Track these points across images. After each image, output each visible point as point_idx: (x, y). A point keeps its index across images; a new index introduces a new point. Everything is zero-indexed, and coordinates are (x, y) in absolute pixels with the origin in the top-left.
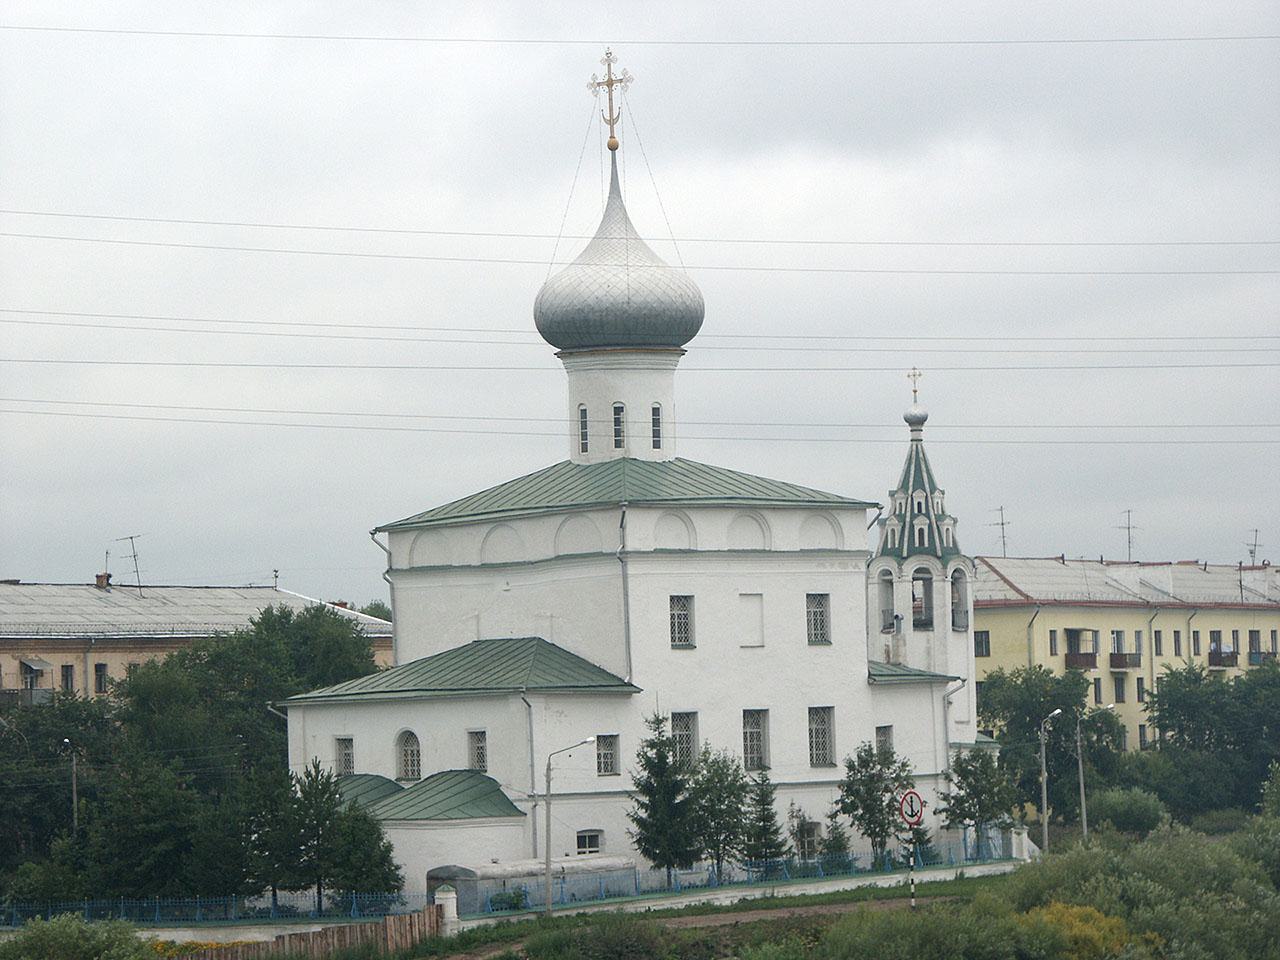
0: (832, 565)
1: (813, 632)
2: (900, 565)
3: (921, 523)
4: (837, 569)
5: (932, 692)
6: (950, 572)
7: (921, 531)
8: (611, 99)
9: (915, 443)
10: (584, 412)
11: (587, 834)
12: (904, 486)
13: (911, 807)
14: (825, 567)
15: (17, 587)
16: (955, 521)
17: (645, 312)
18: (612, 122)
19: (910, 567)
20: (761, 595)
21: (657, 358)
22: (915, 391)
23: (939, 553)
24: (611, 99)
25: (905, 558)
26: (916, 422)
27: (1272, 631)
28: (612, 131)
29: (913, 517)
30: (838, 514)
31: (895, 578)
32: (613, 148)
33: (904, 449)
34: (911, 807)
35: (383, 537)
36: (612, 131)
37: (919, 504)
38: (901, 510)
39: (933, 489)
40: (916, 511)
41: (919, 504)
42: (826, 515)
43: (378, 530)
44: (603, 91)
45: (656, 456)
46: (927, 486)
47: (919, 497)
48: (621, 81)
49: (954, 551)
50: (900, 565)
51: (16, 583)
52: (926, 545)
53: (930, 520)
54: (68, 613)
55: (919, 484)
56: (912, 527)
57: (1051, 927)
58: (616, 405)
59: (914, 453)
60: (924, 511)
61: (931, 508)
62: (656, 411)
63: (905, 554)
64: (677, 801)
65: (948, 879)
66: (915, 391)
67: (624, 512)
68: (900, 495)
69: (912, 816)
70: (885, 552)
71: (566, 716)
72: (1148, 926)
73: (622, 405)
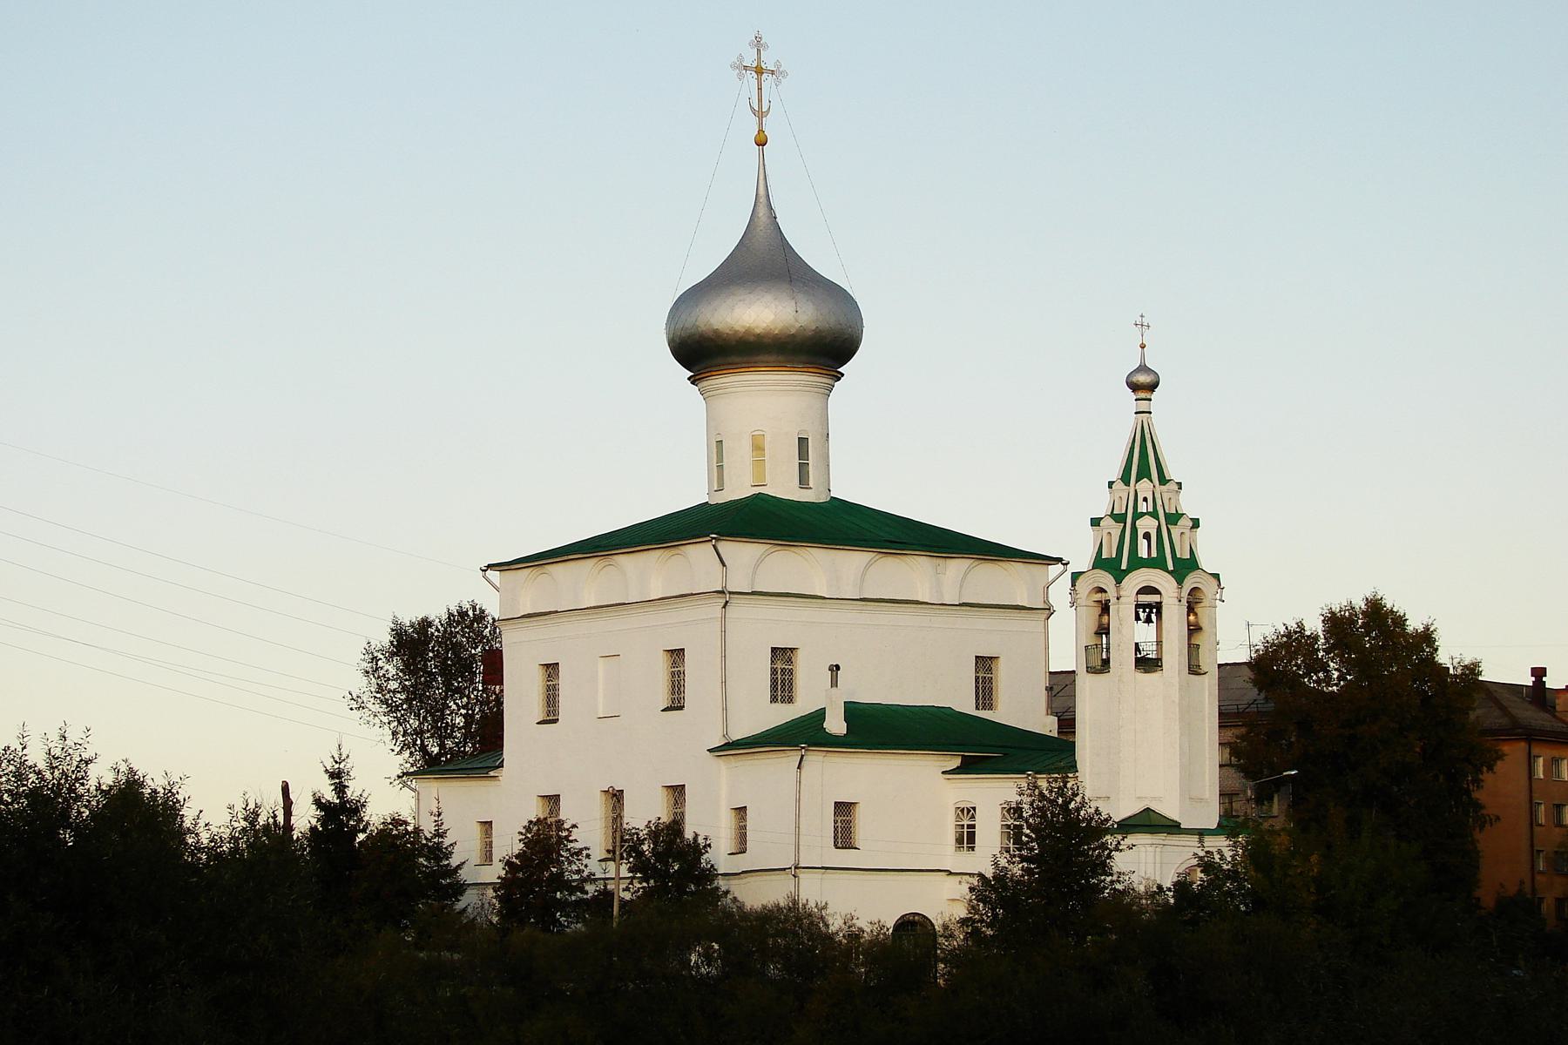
2: (1119, 582)
8: (760, 89)
10: (798, 768)
12: (1125, 478)
16: (1196, 524)
18: (760, 114)
22: (1143, 347)
23: (1171, 567)
24: (760, 89)
26: (1143, 386)
28: (761, 124)
32: (761, 143)
35: (494, 575)
36: (761, 124)
39: (1163, 480)
43: (489, 566)
44: (751, 77)
47: (1145, 488)
48: (773, 72)
50: (1119, 582)
52: (1154, 554)
53: (1158, 519)
55: (1144, 473)
56: (1134, 529)
64: (282, 823)
66: (1143, 347)
67: (802, 756)
68: (1119, 485)
70: (1100, 563)
73: (762, 433)
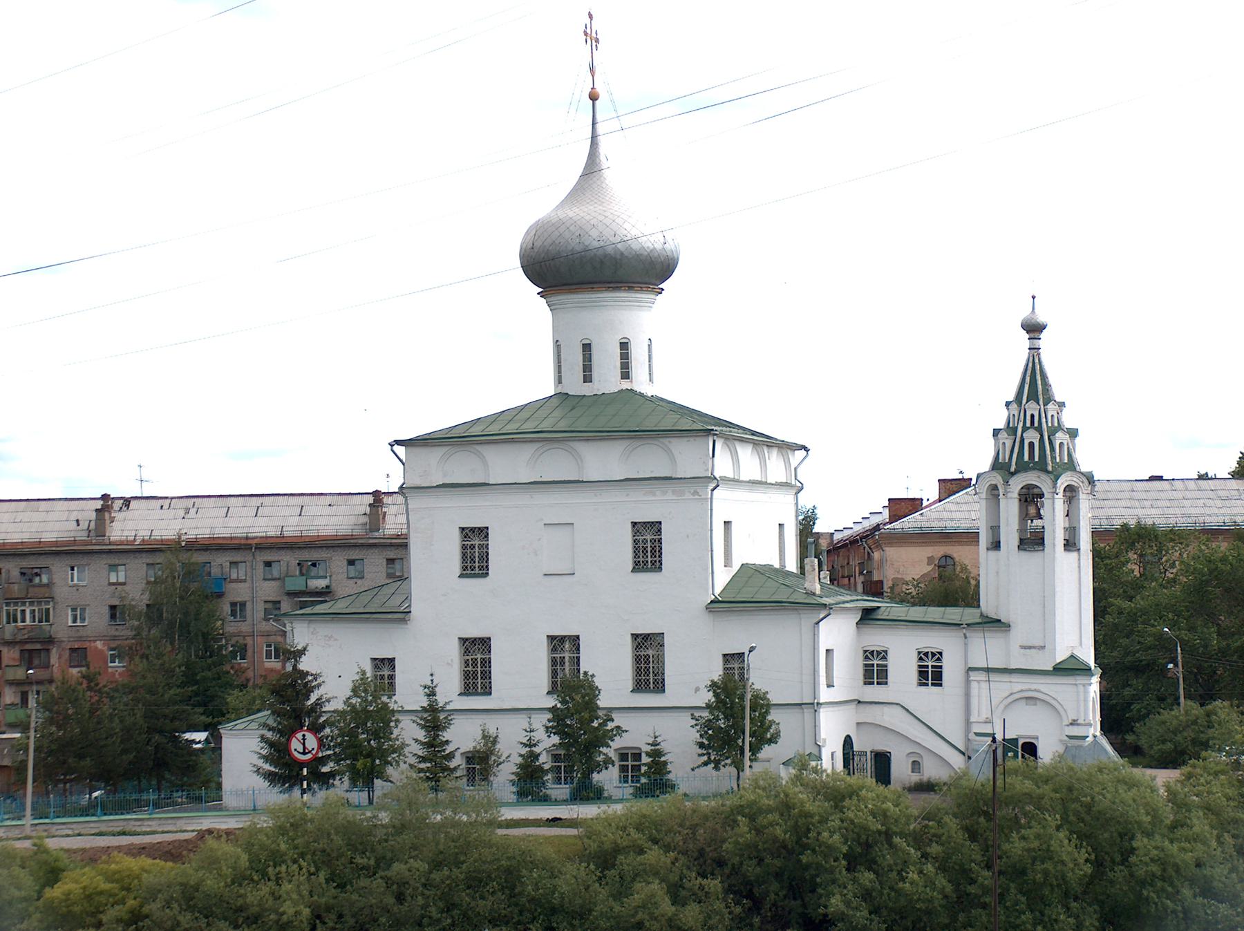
0: (665, 493)
1: (649, 559)
3: (1032, 436)
4: (670, 496)
5: (800, 619)
6: (1061, 490)
7: (1031, 445)
9: (1033, 351)
11: (630, 752)
13: (304, 744)
14: (654, 495)
15: (1162, 482)
17: (542, 256)
19: (1018, 483)
20: (573, 524)
21: (580, 296)
23: (1050, 468)
25: (1013, 474)
26: (1034, 329)
27: (657, 566)
29: (1025, 429)
30: (670, 442)
31: (1001, 491)
33: (1023, 355)
34: (304, 744)
37: (1032, 416)
38: (1014, 424)
39: (1048, 399)
40: (1028, 424)
41: (1032, 416)
42: (656, 442)
45: (587, 389)
46: (1041, 397)
47: (1032, 408)
49: (1071, 466)
51: (1160, 478)
54: (1205, 506)
55: (1033, 396)
56: (1022, 440)
57: (137, 872)
58: (584, 342)
59: (1030, 365)
60: (1036, 424)
61: (1044, 420)
62: (587, 347)
63: (1012, 469)
65: (530, 818)
69: (304, 753)
71: (336, 640)
72: (656, 874)
